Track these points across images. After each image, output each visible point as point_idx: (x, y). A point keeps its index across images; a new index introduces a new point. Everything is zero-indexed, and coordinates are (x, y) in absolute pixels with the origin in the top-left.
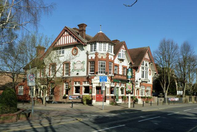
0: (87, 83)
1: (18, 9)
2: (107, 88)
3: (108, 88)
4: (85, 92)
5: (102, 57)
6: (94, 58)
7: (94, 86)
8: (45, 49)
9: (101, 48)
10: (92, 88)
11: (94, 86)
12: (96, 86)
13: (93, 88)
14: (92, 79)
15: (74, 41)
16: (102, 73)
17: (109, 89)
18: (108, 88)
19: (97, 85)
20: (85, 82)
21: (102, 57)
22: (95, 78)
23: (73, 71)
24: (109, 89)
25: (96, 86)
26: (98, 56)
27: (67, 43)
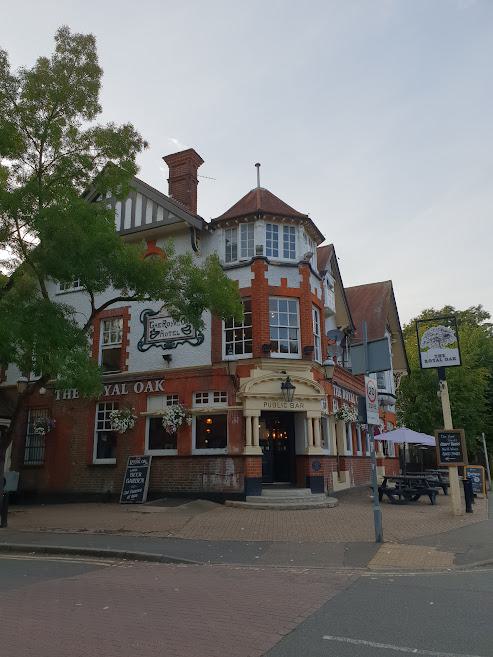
0: (216, 400)
1: (4, 86)
2: (310, 422)
3: (313, 420)
4: (198, 447)
5: (284, 281)
6: (249, 285)
7: (253, 409)
8: (323, 239)
9: (276, 245)
10: (245, 419)
11: (253, 409)
12: (262, 412)
13: (249, 421)
14: (242, 381)
15: (160, 218)
16: (239, 351)
17: (256, 421)
18: (313, 420)
19: (267, 408)
20: (206, 395)
21: (284, 281)
22: (256, 373)
23: (145, 347)
24: (317, 423)
25: (262, 412)
26: (267, 275)
27: (127, 226)
